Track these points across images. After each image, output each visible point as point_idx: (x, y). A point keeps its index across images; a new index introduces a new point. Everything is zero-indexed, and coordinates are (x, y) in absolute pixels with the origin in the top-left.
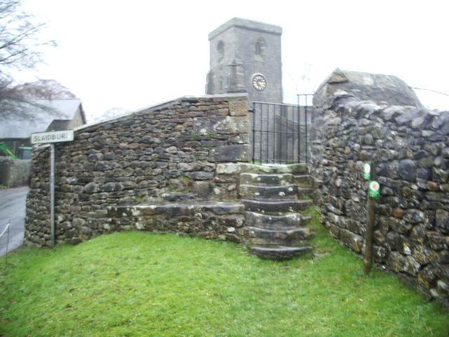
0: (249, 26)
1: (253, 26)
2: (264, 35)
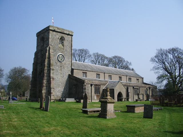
0: (57, 30)
1: (59, 31)
2: (63, 35)
